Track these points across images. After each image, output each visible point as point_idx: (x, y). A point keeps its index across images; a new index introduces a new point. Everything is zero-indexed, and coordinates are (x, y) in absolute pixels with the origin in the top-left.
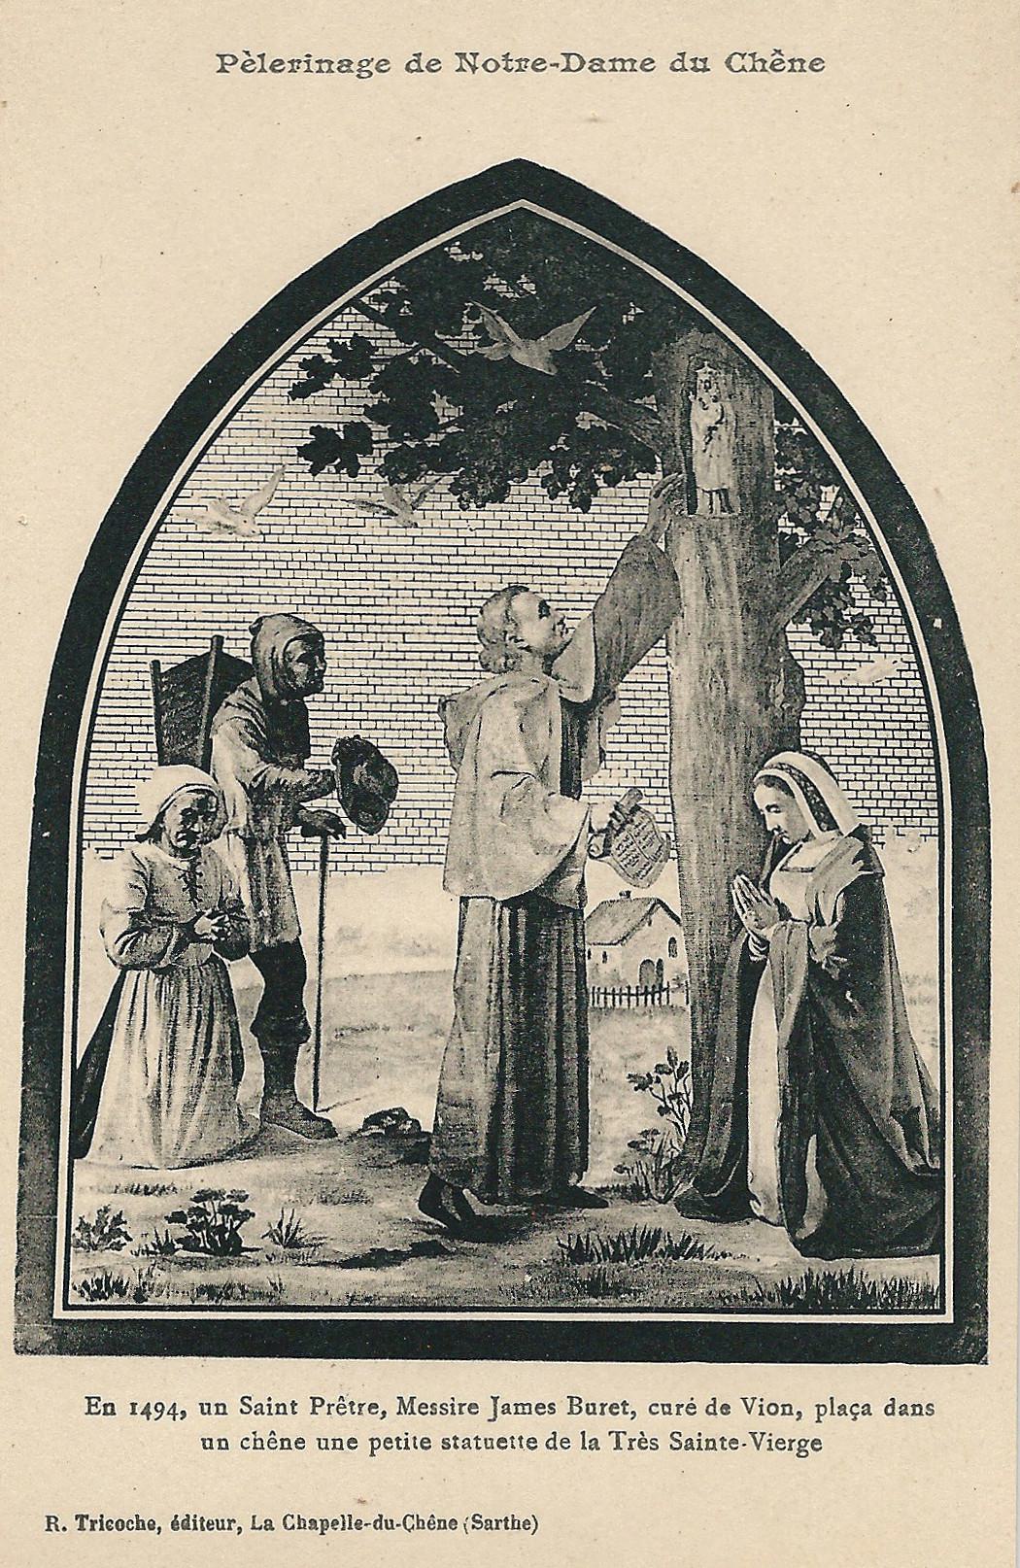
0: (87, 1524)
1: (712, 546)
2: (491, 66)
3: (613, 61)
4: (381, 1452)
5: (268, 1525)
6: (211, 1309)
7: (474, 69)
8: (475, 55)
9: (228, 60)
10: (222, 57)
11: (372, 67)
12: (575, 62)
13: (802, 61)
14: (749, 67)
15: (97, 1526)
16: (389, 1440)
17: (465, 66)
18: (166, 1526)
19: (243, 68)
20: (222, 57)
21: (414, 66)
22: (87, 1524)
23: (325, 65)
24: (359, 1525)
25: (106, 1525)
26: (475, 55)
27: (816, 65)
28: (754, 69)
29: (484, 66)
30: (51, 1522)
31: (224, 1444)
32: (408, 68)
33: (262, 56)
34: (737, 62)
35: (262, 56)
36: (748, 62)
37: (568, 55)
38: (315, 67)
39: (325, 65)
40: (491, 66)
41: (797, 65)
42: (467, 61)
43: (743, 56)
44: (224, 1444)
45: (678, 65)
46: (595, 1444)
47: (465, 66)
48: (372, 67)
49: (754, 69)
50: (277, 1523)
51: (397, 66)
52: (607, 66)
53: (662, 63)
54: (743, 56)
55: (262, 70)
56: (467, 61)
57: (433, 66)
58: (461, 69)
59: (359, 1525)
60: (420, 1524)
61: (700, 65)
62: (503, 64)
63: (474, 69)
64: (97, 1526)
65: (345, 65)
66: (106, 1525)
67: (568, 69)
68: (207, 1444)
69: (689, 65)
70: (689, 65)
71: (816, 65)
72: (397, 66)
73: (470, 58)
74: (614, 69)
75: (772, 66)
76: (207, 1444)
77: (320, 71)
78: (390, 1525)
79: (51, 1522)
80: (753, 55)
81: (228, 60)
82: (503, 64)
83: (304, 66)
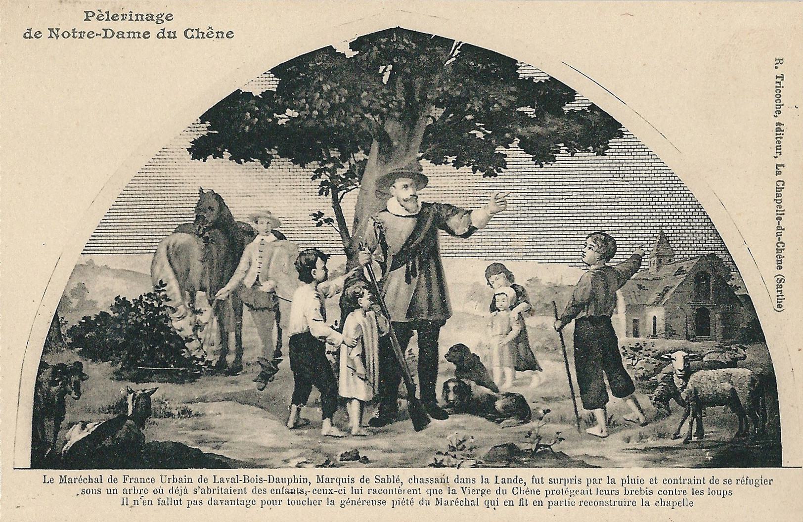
0: (779, 80)
1: (370, 280)
2: (66, 35)
3: (129, 33)
5: (778, 173)
7: (57, 37)
8: (58, 30)
9: (90, 14)
10: (87, 12)
11: (163, 18)
12: (109, 34)
13: (142, 15)
14: (195, 36)
15: (778, 85)
17: (53, 35)
19: (98, 18)
20: (87, 12)
21: (28, 35)
22: (779, 80)
24: (779, 219)
25: (778, 90)
26: (58, 30)
27: (230, 35)
28: (198, 37)
30: (780, 61)
34: (189, 34)
35: (107, 13)
36: (195, 33)
37: (106, 30)
38: (134, 18)
40: (66, 35)
42: (53, 33)
43: (192, 31)
45: (161, 35)
47: (53, 35)
48: (163, 18)
49: (198, 37)
50: (779, 177)
52: (126, 35)
55: (108, 20)
56: (53, 33)
57: (38, 35)
58: (51, 37)
59: (779, 219)
60: (779, 251)
63: (57, 37)
66: (778, 90)
67: (106, 37)
69: (166, 35)
71: (230, 35)
73: (55, 31)
77: (137, 20)
79: (780, 61)
80: (198, 30)
81: (90, 14)
82: (60, 34)
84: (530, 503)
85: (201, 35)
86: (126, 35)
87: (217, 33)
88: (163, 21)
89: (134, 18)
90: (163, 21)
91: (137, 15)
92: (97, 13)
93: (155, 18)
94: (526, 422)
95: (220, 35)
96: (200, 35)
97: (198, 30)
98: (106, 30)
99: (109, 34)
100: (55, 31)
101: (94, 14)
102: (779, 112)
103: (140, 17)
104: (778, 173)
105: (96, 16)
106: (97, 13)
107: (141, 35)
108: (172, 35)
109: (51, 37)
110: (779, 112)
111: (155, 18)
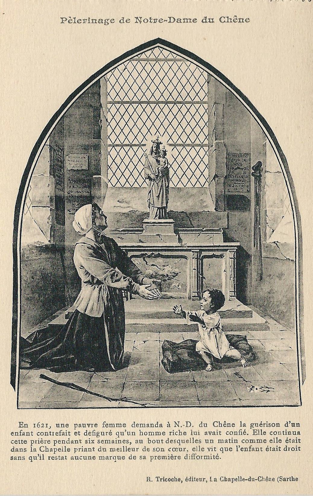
0: (159, 479)
2: (146, 21)
7: (141, 22)
8: (141, 18)
9: (64, 19)
11: (109, 21)
14: (226, 21)
22: (159, 479)
26: (141, 18)
28: (228, 22)
30: (148, 479)
34: (223, 20)
36: (226, 19)
40: (146, 21)
48: (109, 21)
49: (228, 22)
52: (182, 21)
55: (75, 22)
58: (136, 22)
63: (141, 22)
67: (170, 22)
69: (208, 20)
73: (139, 19)
81: (64, 19)
82: (142, 20)
84: (46, 458)
87: (240, 19)
92: (68, 19)
93: (103, 21)
94: (249, 201)
95: (241, 20)
96: (229, 21)
97: (228, 17)
98: (170, 18)
99: (172, 20)
100: (139, 19)
101: (66, 19)
102: (179, 480)
103: (94, 21)
105: (67, 21)
106: (68, 19)
107: (191, 21)
108: (211, 21)
109: (136, 22)
110: (179, 480)
111: (103, 21)
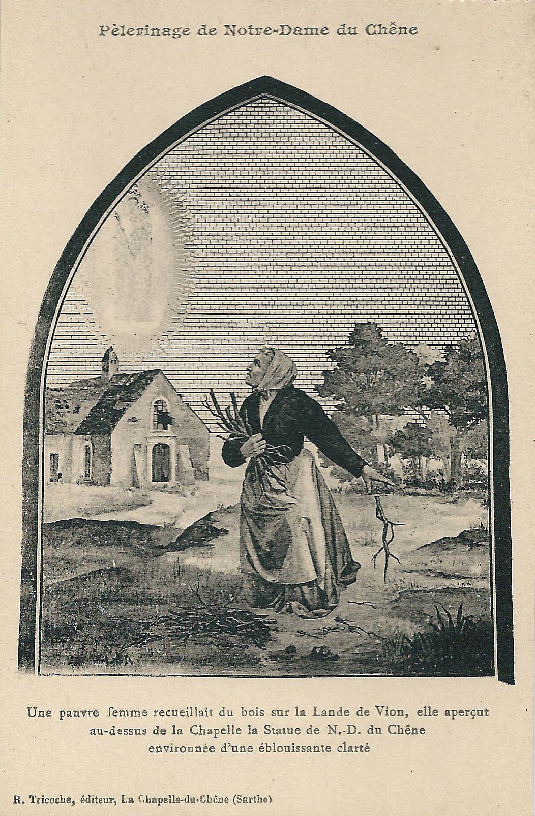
0: (35, 800)
2: (242, 31)
4: (457, 717)
5: (131, 800)
6: (40, 629)
8: (234, 26)
12: (286, 30)
13: (158, 30)
15: (41, 801)
16: (461, 711)
17: (229, 32)
18: (78, 801)
22: (35, 800)
23: (155, 32)
26: (234, 26)
27: (413, 31)
28: (380, 33)
29: (239, 31)
30: (17, 799)
31: (100, 732)
32: (367, 30)
33: (123, 27)
34: (371, 30)
35: (123, 27)
36: (377, 29)
39: (155, 32)
40: (242, 31)
41: (314, 31)
42: (231, 30)
43: (374, 26)
44: (100, 732)
45: (341, 31)
46: (255, 731)
47: (229, 32)
48: (180, 32)
51: (194, 31)
53: (333, 30)
54: (374, 26)
55: (123, 34)
56: (231, 30)
61: (353, 31)
62: (248, 31)
63: (234, 33)
64: (41, 801)
65: (166, 32)
67: (283, 33)
68: (93, 732)
69: (347, 31)
70: (347, 31)
71: (413, 31)
72: (194, 31)
74: (307, 34)
75: (410, 31)
76: (93, 732)
78: (193, 800)
79: (17, 799)
80: (380, 26)
81: (105, 28)
82: (248, 31)
83: (144, 32)
85: (382, 30)
86: (304, 32)
88: (180, 36)
89: (150, 32)
90: (180, 36)
91: (153, 30)
93: (171, 32)
99: (286, 30)
104: (131, 800)
105: (111, 30)
111: (171, 32)
